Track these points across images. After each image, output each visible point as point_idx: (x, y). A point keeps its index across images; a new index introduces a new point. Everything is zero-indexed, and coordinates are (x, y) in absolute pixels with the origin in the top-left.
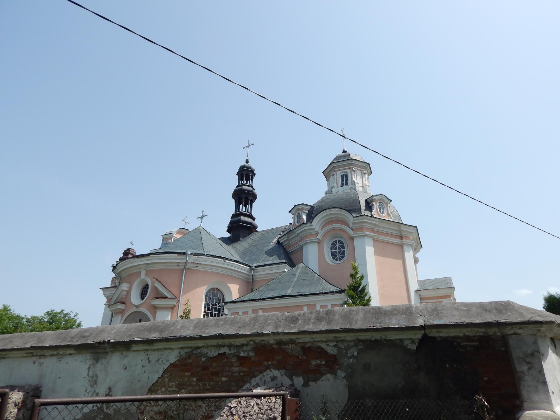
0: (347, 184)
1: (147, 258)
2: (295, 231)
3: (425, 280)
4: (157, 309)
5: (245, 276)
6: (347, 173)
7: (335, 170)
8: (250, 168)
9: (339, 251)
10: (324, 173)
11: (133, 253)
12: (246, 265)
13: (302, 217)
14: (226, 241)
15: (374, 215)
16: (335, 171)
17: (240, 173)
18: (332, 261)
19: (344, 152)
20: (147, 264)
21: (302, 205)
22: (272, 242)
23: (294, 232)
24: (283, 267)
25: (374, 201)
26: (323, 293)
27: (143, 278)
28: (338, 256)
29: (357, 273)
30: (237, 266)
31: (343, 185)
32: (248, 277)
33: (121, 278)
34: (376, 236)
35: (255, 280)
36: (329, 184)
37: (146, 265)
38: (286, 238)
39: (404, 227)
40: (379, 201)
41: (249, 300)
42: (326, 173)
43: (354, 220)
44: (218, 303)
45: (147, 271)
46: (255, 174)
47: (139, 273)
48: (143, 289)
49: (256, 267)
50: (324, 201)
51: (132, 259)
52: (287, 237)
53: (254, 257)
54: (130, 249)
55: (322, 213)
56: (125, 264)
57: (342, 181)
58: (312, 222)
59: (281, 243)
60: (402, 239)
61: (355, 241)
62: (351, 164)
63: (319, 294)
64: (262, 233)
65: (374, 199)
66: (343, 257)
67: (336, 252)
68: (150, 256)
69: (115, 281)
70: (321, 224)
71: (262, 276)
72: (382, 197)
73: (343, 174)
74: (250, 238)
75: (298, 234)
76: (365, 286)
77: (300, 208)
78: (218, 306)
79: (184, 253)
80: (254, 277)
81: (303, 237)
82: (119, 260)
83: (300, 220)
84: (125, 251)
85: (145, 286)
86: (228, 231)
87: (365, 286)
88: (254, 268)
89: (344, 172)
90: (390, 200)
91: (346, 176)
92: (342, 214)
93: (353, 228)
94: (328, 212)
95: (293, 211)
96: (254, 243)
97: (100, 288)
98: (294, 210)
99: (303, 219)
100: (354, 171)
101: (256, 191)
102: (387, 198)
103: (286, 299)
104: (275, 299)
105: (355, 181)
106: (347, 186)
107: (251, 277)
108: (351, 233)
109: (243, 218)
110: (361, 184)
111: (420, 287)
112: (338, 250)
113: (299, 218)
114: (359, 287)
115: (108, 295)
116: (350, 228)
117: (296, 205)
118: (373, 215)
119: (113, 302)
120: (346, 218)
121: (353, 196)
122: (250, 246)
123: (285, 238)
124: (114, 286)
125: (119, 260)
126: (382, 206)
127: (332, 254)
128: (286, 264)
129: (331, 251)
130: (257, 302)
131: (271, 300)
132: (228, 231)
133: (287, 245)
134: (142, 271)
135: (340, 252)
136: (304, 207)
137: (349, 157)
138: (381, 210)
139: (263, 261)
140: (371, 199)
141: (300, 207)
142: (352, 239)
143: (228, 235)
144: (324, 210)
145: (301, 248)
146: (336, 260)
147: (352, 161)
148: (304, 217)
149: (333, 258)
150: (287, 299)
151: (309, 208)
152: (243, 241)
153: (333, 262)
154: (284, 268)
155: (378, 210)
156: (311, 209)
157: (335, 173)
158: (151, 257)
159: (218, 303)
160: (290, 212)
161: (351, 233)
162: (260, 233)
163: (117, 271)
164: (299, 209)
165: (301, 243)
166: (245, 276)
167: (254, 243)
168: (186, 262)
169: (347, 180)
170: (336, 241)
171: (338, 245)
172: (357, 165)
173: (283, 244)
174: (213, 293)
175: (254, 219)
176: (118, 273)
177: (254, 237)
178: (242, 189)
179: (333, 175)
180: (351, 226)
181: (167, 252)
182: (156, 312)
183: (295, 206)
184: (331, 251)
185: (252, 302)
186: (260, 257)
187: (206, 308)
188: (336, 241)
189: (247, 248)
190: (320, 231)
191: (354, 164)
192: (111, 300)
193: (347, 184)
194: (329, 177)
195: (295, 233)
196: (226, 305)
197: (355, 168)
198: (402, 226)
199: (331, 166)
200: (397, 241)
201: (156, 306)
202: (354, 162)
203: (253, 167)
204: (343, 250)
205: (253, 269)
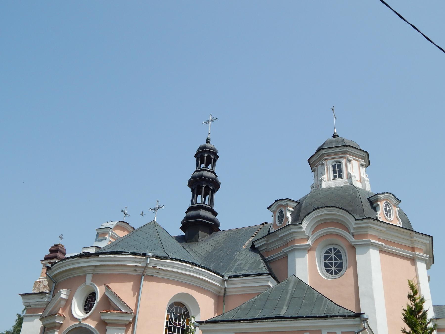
0: (340, 176)
1: (96, 258)
2: (277, 233)
3: (440, 306)
4: (107, 326)
5: (215, 288)
6: (341, 163)
7: (325, 158)
8: (213, 149)
9: (334, 262)
10: (310, 161)
11: (63, 250)
12: (218, 274)
13: (286, 214)
14: (180, 239)
15: (380, 218)
16: (324, 160)
17: (200, 155)
18: (325, 275)
19: (335, 136)
20: (96, 266)
21: (286, 200)
22: (243, 245)
23: (276, 234)
24: (266, 279)
25: (379, 200)
26: (331, 317)
27: (89, 284)
28: (333, 269)
29: (416, 293)
30: (208, 275)
31: (335, 177)
32: (219, 290)
33: (56, 282)
34: (383, 245)
35: (228, 294)
36: (316, 175)
37: (93, 268)
38: (264, 241)
39: (417, 237)
40: (385, 201)
41: (232, 321)
42: (312, 161)
43: (356, 224)
44: (181, 322)
45: (94, 275)
46: (218, 157)
47: (84, 277)
48: (87, 298)
49: (230, 277)
50: (314, 197)
51: (76, 259)
52: (267, 241)
53: (222, 264)
54: (59, 245)
55: (314, 212)
56: (68, 263)
57: (334, 172)
58: (301, 224)
59: (257, 248)
60: (414, 251)
61: (357, 250)
62: (345, 152)
63: (326, 317)
64: (227, 233)
65: (379, 199)
66: (340, 271)
67: (331, 264)
68: (100, 256)
69: (39, 285)
70: (313, 226)
71: (240, 289)
72: (390, 196)
73: (335, 163)
74: (212, 238)
75: (281, 238)
76: (427, 311)
77: (284, 204)
78: (181, 326)
79: (144, 255)
80: (227, 290)
81: (288, 241)
82: (44, 259)
83: (282, 220)
84: (52, 247)
85: (90, 295)
86: (182, 228)
87: (427, 311)
88: (227, 278)
89: (337, 162)
90: (398, 200)
91: (340, 166)
92: (341, 216)
93: (354, 234)
94: (320, 213)
95: (274, 208)
96: (219, 246)
97: (20, 295)
98: (275, 206)
99: (287, 219)
100: (350, 161)
101: (219, 179)
102: (395, 197)
103: (281, 322)
104: (267, 321)
105: (352, 174)
106: (340, 179)
107: (223, 291)
108: (352, 240)
109: (203, 213)
110: (358, 179)
111: (436, 314)
112: (333, 261)
113: (282, 216)
114: (419, 312)
115: (29, 304)
116: (350, 233)
117: (278, 200)
118: (378, 218)
119: (47, 314)
120: (345, 221)
121: (351, 192)
122: (214, 249)
123: (263, 242)
124: (37, 292)
125: (45, 258)
126: (389, 207)
127: (326, 266)
128: (270, 276)
129: (325, 262)
130: (243, 324)
131: (247, 322)
132: (182, 228)
133: (265, 251)
134: (87, 275)
135: (336, 263)
136: (289, 203)
137: (343, 143)
138: (388, 213)
139: (236, 270)
140: (375, 198)
141: (283, 203)
142: (353, 248)
143: (183, 233)
144: (316, 209)
145: (285, 257)
146: (331, 273)
147: (347, 148)
148: (289, 215)
149: (328, 271)
150: (283, 322)
151: (295, 204)
152: (203, 242)
153: (327, 276)
154: (268, 281)
155: (385, 212)
156: (296, 206)
157: (325, 161)
158: (101, 257)
159: (181, 322)
160: (268, 208)
161: (352, 240)
162: (225, 234)
163: (53, 272)
164: (281, 205)
165: (285, 250)
166: (215, 288)
167: (219, 246)
168: (146, 267)
169: (340, 171)
170: (331, 248)
171: (333, 254)
172: (351, 152)
173: (260, 250)
174: (177, 309)
175: (215, 214)
176: (52, 276)
177: (216, 237)
178: (202, 176)
179: (323, 164)
180: (352, 231)
181: (122, 252)
182: (106, 330)
183: (276, 201)
184: (325, 262)
185: (236, 323)
186: (231, 265)
187: (168, 328)
188: (330, 250)
189: (210, 251)
190: (310, 235)
191: (350, 152)
192: (45, 311)
193: (340, 176)
194: (317, 166)
195: (278, 236)
196: (200, 325)
197: (350, 158)
198: (415, 234)
199: (320, 152)
200: (408, 253)
201: (106, 321)
202: (349, 149)
203: (217, 148)
204: (340, 261)
205: (227, 280)
